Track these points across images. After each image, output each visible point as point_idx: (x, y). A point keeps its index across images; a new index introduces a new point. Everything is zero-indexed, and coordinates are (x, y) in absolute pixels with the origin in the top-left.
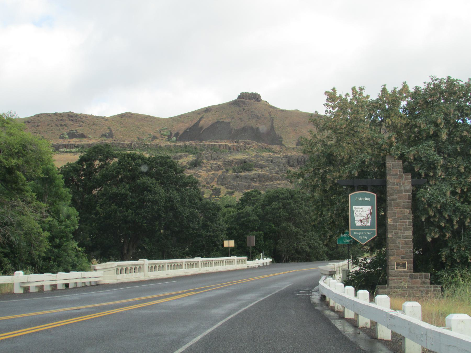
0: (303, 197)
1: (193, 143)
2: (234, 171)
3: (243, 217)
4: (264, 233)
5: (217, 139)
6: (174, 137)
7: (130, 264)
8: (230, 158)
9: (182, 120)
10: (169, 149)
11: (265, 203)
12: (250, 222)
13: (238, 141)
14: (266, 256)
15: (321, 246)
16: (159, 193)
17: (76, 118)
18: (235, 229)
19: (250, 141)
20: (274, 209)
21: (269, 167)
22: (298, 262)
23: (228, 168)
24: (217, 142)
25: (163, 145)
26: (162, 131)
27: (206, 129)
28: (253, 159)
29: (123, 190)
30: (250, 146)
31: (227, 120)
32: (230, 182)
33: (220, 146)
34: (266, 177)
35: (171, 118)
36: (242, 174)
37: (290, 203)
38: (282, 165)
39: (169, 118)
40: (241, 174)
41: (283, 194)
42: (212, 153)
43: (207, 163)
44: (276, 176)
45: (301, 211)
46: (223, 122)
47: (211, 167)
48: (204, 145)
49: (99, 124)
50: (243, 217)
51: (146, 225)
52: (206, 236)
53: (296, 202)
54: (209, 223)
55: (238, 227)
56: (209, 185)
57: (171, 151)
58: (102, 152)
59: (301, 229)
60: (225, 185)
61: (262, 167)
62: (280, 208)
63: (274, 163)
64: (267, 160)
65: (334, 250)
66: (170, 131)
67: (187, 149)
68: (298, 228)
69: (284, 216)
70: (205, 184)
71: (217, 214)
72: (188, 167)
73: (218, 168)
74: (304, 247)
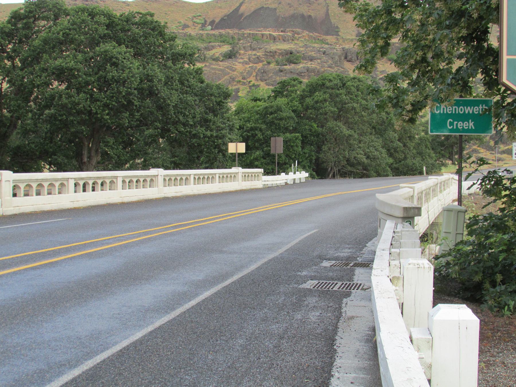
0: (359, 85)
1: (231, 32)
2: (278, 63)
3: (271, 113)
4: (302, 136)
5: (260, 28)
6: (209, 25)
7: (27, 178)
8: (272, 48)
9: (219, 5)
10: (200, 38)
11: (306, 93)
12: (281, 119)
13: (285, 30)
14: (304, 168)
15: (384, 155)
16: (130, 68)
17: (92, 3)
18: (261, 130)
19: (300, 30)
20: (317, 102)
21: (320, 59)
22: (349, 178)
23: (269, 60)
24: (259, 31)
25: (193, 33)
26: (194, 18)
27: (247, 16)
28: (302, 49)
29: (73, 62)
30: (300, 36)
31: (273, 6)
32: (271, 77)
33: (263, 35)
34: (317, 71)
35: (206, 3)
36: (287, 67)
37: (341, 94)
38: (337, 58)
39: (204, 3)
40: (285, 67)
41: (330, 81)
42: (252, 42)
43: (244, 54)
44: (329, 70)
45: (355, 105)
46: (268, 8)
47: (249, 59)
48: (244, 34)
49: (120, 10)
50: (271, 113)
51: (108, 117)
52: (205, 136)
53: (349, 92)
54: (210, 116)
55: (264, 127)
56: (245, 81)
57: (203, 40)
58: (45, 5)
59: (355, 132)
60: (266, 80)
61: (312, 59)
62: (325, 100)
63: (327, 54)
64: (319, 51)
65: (400, 162)
66: (204, 18)
67: (222, 39)
68: (352, 129)
69: (331, 112)
70: (240, 79)
71: (223, 103)
72: (222, 58)
73: (258, 60)
74: (359, 156)
